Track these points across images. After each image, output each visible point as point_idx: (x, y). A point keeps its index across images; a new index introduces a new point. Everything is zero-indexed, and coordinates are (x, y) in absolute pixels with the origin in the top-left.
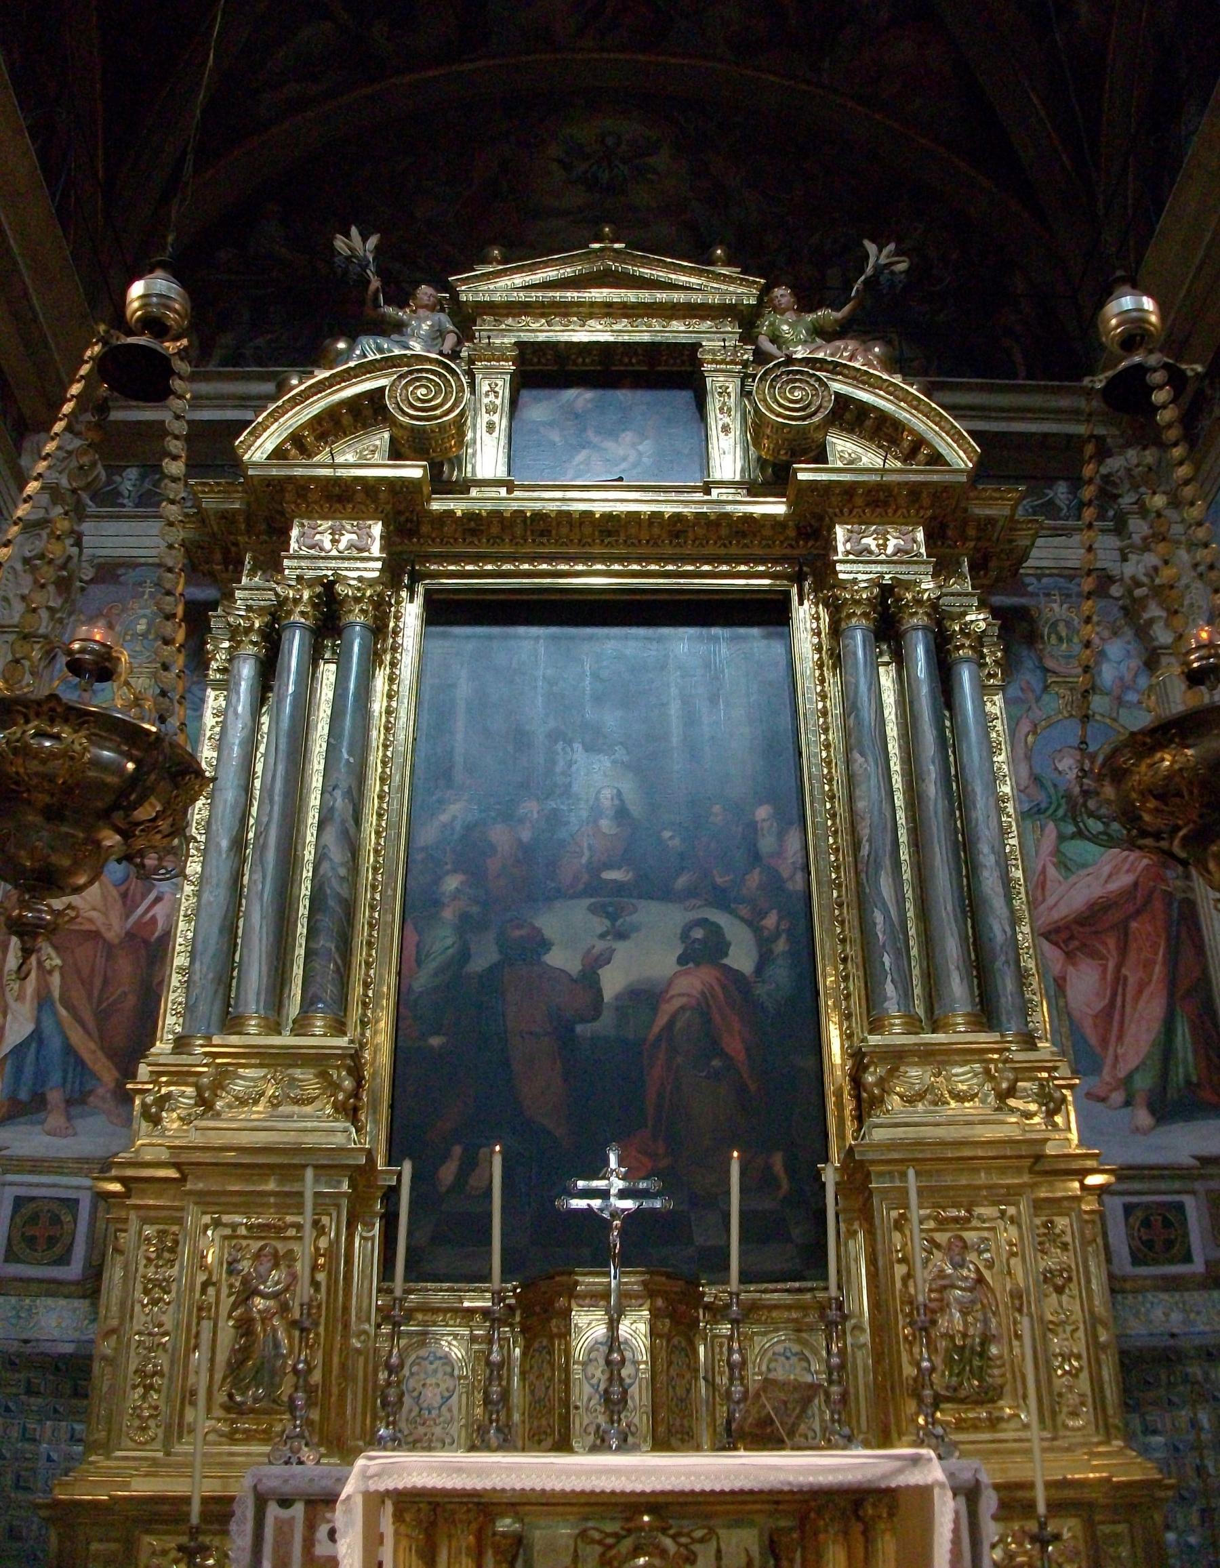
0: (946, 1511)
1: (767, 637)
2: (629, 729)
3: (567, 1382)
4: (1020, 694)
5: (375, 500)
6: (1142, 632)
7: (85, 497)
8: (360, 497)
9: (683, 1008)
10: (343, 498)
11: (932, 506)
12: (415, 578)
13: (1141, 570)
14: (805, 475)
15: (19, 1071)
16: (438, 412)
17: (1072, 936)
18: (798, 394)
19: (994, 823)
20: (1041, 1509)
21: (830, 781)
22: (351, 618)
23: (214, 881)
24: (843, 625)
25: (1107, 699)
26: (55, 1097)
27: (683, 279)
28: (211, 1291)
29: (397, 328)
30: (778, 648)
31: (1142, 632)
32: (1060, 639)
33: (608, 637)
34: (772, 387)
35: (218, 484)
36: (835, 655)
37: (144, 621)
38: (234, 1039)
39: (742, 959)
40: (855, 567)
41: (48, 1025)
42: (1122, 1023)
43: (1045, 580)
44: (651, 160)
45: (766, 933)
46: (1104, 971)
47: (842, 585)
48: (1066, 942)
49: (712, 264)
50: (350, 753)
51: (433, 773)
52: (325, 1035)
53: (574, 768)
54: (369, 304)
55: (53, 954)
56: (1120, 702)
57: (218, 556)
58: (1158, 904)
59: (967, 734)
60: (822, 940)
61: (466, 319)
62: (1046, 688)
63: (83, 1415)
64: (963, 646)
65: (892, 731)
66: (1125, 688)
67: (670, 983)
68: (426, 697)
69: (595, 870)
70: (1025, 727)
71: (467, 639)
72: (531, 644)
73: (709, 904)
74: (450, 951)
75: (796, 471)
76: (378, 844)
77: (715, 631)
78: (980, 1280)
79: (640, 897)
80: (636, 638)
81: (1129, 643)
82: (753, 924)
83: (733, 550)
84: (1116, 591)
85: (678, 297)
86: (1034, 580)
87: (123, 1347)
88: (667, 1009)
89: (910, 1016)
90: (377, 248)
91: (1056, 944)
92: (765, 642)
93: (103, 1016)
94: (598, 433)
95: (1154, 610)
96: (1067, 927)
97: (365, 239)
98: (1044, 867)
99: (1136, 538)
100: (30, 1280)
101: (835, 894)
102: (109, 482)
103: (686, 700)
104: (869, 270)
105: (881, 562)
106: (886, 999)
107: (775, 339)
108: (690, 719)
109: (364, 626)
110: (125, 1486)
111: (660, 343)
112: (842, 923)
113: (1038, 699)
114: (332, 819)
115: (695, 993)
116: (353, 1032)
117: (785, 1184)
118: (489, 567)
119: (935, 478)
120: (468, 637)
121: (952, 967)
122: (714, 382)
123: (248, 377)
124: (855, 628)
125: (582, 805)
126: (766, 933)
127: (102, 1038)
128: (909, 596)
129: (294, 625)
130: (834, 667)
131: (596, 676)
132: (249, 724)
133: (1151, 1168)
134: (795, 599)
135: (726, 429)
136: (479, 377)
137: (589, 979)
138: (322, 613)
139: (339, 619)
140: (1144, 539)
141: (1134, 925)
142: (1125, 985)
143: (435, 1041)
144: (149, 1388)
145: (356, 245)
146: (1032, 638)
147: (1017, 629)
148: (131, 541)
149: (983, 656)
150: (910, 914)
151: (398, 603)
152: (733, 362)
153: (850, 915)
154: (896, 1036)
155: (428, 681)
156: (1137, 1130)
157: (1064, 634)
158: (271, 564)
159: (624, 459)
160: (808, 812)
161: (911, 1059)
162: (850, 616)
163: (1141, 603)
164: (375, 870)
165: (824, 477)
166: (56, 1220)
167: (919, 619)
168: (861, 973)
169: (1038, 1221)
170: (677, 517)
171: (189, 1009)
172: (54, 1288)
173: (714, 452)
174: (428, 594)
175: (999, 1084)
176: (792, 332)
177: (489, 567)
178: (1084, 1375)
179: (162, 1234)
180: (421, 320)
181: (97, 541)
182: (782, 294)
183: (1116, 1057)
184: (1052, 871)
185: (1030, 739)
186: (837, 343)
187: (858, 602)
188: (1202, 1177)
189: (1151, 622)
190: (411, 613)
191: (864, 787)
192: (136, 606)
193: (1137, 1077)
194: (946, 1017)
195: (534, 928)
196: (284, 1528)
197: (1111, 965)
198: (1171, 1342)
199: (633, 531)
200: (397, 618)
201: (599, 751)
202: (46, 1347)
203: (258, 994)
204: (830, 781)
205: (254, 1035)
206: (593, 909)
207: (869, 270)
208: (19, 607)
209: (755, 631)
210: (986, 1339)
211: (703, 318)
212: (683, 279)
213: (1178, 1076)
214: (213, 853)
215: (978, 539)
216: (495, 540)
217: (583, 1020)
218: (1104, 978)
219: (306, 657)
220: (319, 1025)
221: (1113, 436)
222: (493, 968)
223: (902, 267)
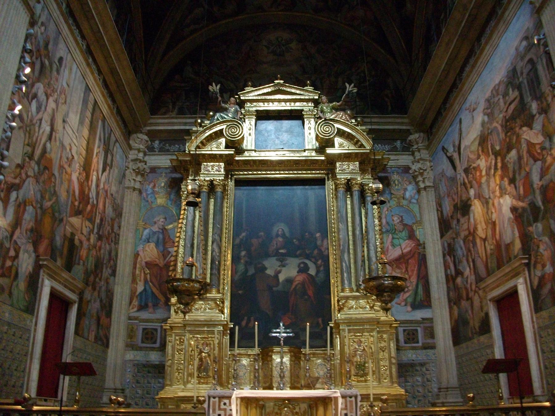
0: (340, 400)
3: (272, 371)
6: (417, 183)
9: (299, 284)
10: (214, 158)
15: (141, 299)
20: (372, 399)
26: (150, 304)
28: (193, 352)
29: (225, 110)
31: (417, 183)
32: (396, 185)
39: (312, 271)
41: (147, 288)
43: (393, 169)
44: (290, 45)
56: (410, 202)
57: (182, 169)
58: (416, 256)
61: (241, 104)
63: (163, 378)
67: (295, 278)
69: (277, 250)
71: (245, 191)
72: (261, 190)
77: (307, 187)
78: (364, 349)
79: (288, 256)
82: (315, 263)
83: (311, 168)
87: (173, 363)
90: (220, 88)
97: (216, 86)
100: (147, 347)
102: (152, 144)
104: (347, 92)
107: (322, 111)
110: (176, 393)
117: (322, 326)
119: (362, 151)
123: (186, 118)
133: (410, 321)
140: (418, 159)
143: (240, 292)
144: (179, 373)
145: (215, 88)
148: (159, 161)
154: (347, 293)
156: (408, 312)
158: (197, 172)
163: (417, 176)
166: (152, 333)
169: (379, 335)
172: (153, 349)
178: (388, 370)
179: (180, 339)
180: (232, 108)
184: (390, 247)
188: (423, 323)
189: (419, 181)
190: (231, 184)
196: (214, 403)
198: (413, 362)
202: (152, 363)
206: (277, 260)
207: (347, 92)
208: (132, 181)
209: (317, 187)
210: (365, 363)
213: (418, 298)
214: (186, 248)
217: (275, 287)
222: (253, 275)
223: (355, 91)
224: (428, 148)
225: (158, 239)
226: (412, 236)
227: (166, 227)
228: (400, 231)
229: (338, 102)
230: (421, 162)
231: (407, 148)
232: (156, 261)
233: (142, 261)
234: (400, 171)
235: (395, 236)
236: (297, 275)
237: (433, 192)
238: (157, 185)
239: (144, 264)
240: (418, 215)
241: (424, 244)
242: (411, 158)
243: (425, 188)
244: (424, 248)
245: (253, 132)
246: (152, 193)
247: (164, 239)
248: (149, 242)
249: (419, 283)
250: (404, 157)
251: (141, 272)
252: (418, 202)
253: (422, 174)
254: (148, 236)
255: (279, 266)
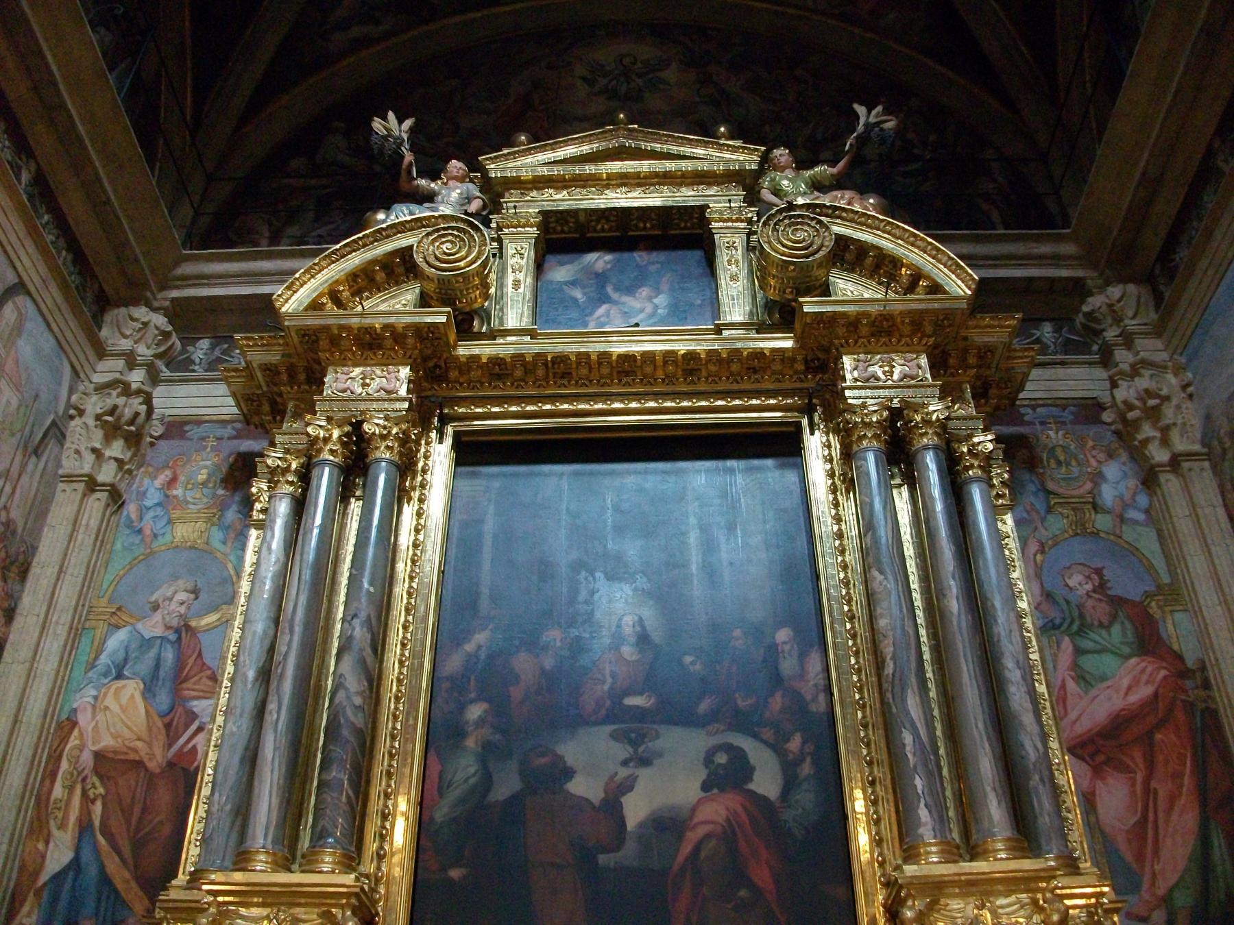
1: (782, 466)
2: (657, 558)
4: (1025, 515)
5: (403, 345)
6: (1137, 454)
7: (160, 364)
8: (389, 343)
9: (708, 836)
11: (934, 334)
12: (444, 420)
13: (1132, 393)
14: (811, 306)
16: (462, 264)
17: (1095, 750)
18: (800, 235)
19: (1016, 638)
21: (849, 602)
22: (378, 454)
23: (238, 711)
24: (855, 448)
25: (1108, 517)
27: (689, 150)
29: (428, 198)
30: (791, 477)
31: (1137, 454)
32: (1059, 463)
33: (629, 473)
34: (775, 230)
35: (262, 338)
36: (847, 479)
37: (204, 471)
38: (238, 876)
39: (767, 783)
40: (863, 393)
41: (87, 855)
42: (1156, 841)
44: (665, 74)
45: (791, 756)
46: (1133, 785)
47: (852, 409)
48: (1092, 756)
49: (719, 138)
50: (371, 584)
51: (458, 602)
52: (333, 872)
53: (596, 597)
54: (404, 174)
55: (98, 784)
56: (1122, 519)
57: (266, 408)
58: (1180, 716)
59: (982, 549)
60: (848, 762)
61: (494, 192)
62: (1049, 510)
64: (972, 467)
65: (909, 550)
66: (1126, 506)
67: (694, 810)
68: (455, 531)
69: (617, 695)
70: (1033, 547)
72: (556, 482)
73: (731, 728)
74: (472, 781)
75: (801, 305)
76: (401, 673)
77: (731, 463)
79: (662, 722)
80: (655, 472)
81: (1124, 464)
82: (777, 748)
83: (746, 386)
84: (1107, 417)
85: (686, 166)
86: (1029, 411)
88: (693, 836)
89: (948, 843)
91: (1083, 759)
92: (777, 473)
93: (138, 845)
94: (616, 289)
95: (1147, 431)
96: (1091, 741)
97: (400, 122)
98: (1063, 681)
99: (1125, 367)
101: (860, 715)
102: (184, 351)
103: (704, 529)
104: (860, 128)
105: (889, 387)
106: (919, 824)
107: (777, 192)
108: (709, 546)
109: (390, 462)
111: (672, 207)
112: (868, 745)
113: (1043, 520)
114: (350, 648)
115: (721, 821)
116: (369, 867)
118: (514, 409)
120: (493, 476)
121: (988, 789)
122: (721, 239)
124: (866, 450)
125: (604, 632)
126: (791, 756)
127: (136, 867)
128: (918, 418)
129: (324, 462)
130: (848, 492)
131: (617, 509)
132: (282, 558)
134: (806, 431)
135: (734, 278)
136: (506, 242)
137: (612, 807)
138: (352, 452)
139: (367, 456)
141: (1158, 736)
142: (1155, 799)
143: (455, 873)
145: (392, 127)
146: (1032, 463)
147: (1019, 452)
148: (200, 402)
149: (991, 479)
150: (939, 733)
151: (428, 444)
152: (738, 220)
153: (877, 736)
154: (932, 864)
155: (458, 517)
157: (1062, 458)
159: (642, 311)
160: (829, 633)
161: (951, 890)
162: (861, 438)
163: (1135, 425)
164: (397, 699)
165: (829, 308)
167: (929, 439)
168: (891, 797)
170: (691, 356)
171: (205, 841)
173: (724, 299)
174: (457, 435)
175: (1049, 916)
176: (791, 184)
177: (514, 409)
181: (169, 403)
182: (781, 154)
183: (1154, 875)
184: (1071, 686)
185: (1039, 557)
186: (835, 193)
187: (868, 425)
189: (1147, 441)
190: (439, 456)
191: (885, 605)
192: (199, 458)
193: (1176, 894)
194: (985, 842)
195: (556, 755)
197: (1139, 777)
199: (649, 370)
200: (426, 457)
201: (620, 580)
203: (267, 828)
204: (849, 602)
205: (262, 871)
206: (615, 736)
207: (860, 128)
208: (89, 458)
209: (769, 462)
211: (710, 184)
212: (689, 150)
214: (239, 684)
215: (979, 367)
216: (519, 383)
218: (1133, 793)
219: (334, 492)
220: (328, 860)
221: (1092, 279)
222: (514, 799)
223: (890, 125)
224: (1158, 331)
225: (157, 666)
226: (1148, 641)
227: (193, 624)
228: (1101, 625)
229: (833, 163)
230: (1147, 373)
231: (1085, 342)
232: (135, 751)
233: (81, 748)
234: (1067, 416)
235: (1086, 644)
236: (700, 802)
237: (1208, 474)
238: (182, 478)
239: (87, 759)
240: (1159, 563)
241: (1203, 668)
242: (1100, 373)
243: (1175, 463)
244: (1206, 685)
245: (527, 280)
246: (159, 504)
247: (180, 664)
248: (119, 676)
249: (1213, 825)
250: (1073, 371)
251: (71, 789)
252: (1157, 519)
253: (1153, 414)
254: (121, 655)
255: (625, 763)
